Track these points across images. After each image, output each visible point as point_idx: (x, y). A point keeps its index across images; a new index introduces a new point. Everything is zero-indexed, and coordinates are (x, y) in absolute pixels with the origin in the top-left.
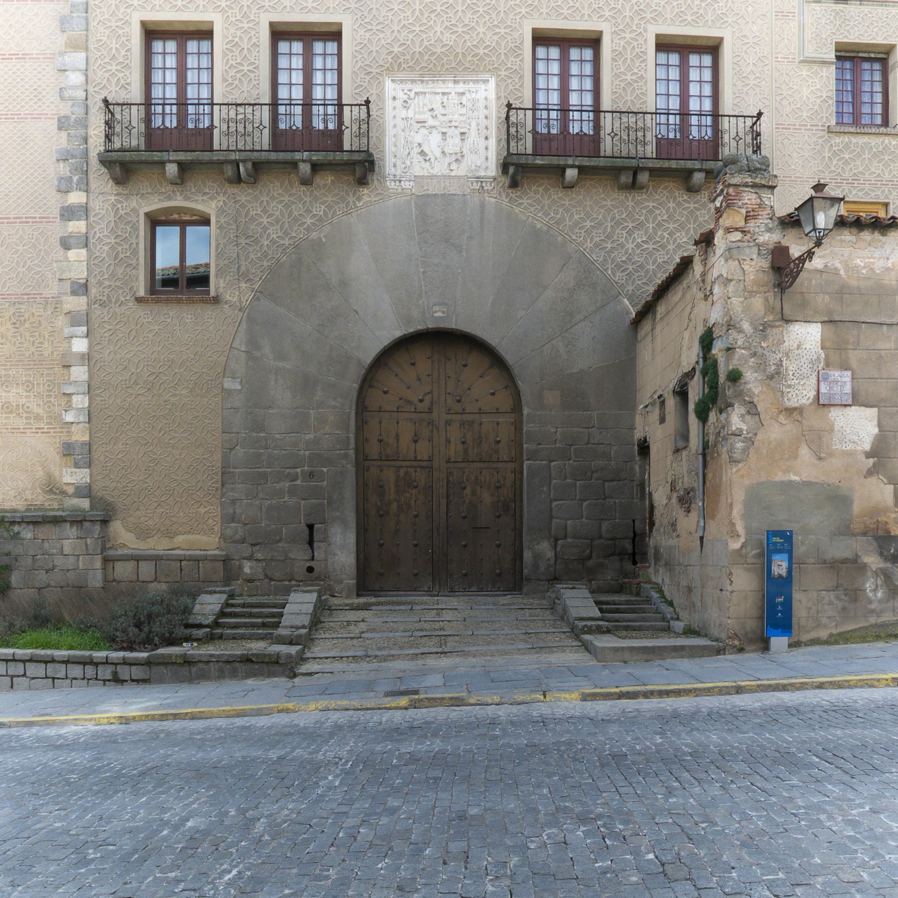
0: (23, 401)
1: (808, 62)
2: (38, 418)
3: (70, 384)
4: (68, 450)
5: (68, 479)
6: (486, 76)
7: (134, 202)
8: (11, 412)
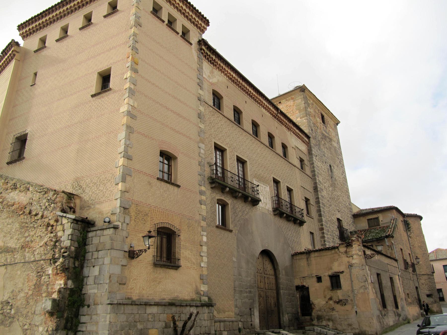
0: (190, 256)
1: (84, 323)
2: (194, 264)
3: (55, 191)
4: (201, 278)
5: (202, 289)
6: (267, 185)
7: (214, 195)
8: (187, 260)
